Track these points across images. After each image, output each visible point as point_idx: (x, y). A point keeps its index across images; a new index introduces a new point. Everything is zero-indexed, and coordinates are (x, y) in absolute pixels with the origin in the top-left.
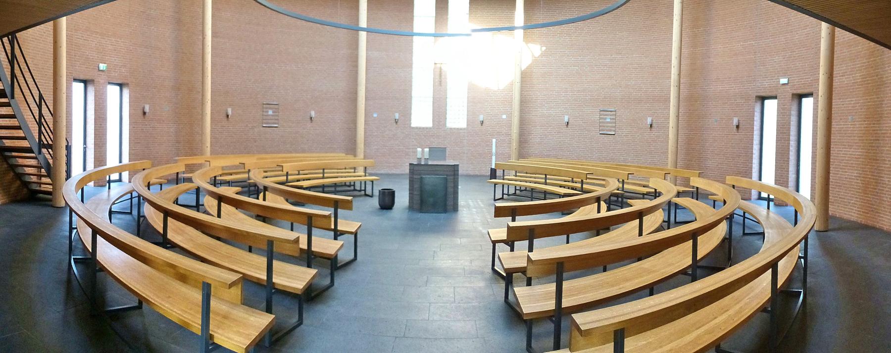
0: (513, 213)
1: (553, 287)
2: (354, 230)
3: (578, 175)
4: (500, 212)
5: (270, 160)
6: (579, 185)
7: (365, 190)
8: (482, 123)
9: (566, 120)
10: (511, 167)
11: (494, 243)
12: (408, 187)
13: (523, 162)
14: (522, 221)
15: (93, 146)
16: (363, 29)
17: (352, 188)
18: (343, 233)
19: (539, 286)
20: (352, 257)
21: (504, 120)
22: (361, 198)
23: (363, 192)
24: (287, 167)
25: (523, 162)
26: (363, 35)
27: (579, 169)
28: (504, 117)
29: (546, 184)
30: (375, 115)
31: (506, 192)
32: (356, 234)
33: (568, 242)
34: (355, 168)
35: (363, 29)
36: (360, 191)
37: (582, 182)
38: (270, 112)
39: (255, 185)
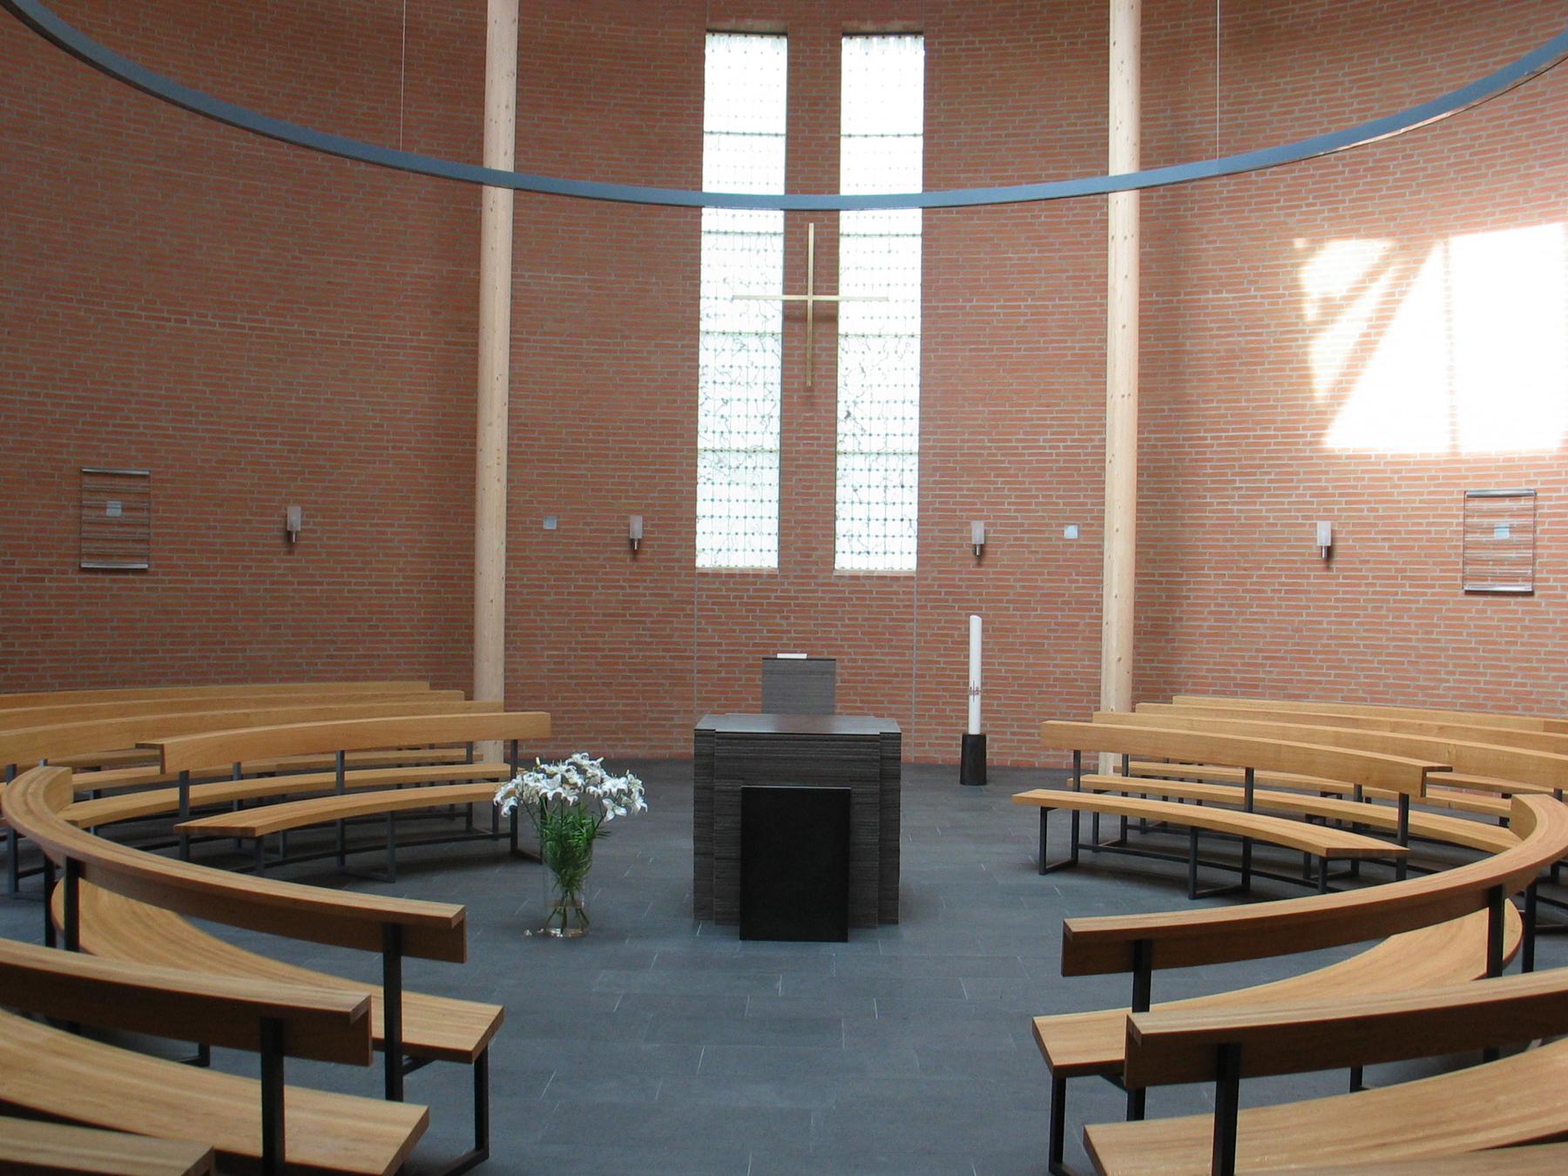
0: (1139, 959)
1: (1205, 1124)
2: (468, 1044)
3: (1386, 775)
4: (1085, 955)
5: (108, 721)
6: (1390, 814)
7: (513, 835)
8: (981, 552)
9: (1323, 536)
10: (1110, 741)
11: (1061, 1075)
12: (688, 815)
13: (1156, 720)
14: (1192, 1008)
15: (511, 114)
16: (499, 179)
17: (460, 824)
18: (425, 1055)
19: (1162, 1122)
20: (467, 1145)
21: (1069, 543)
22: (497, 872)
23: (505, 844)
24: (181, 749)
25: (1156, 720)
26: (499, 206)
27: (1384, 744)
28: (1071, 532)
29: (1249, 806)
30: (550, 524)
31: (1085, 834)
32: (478, 1061)
33: (1077, 754)
34: (470, 746)
35: (499, 179)
36: (496, 836)
37: (1404, 803)
38: (114, 510)
39: (36, 852)
